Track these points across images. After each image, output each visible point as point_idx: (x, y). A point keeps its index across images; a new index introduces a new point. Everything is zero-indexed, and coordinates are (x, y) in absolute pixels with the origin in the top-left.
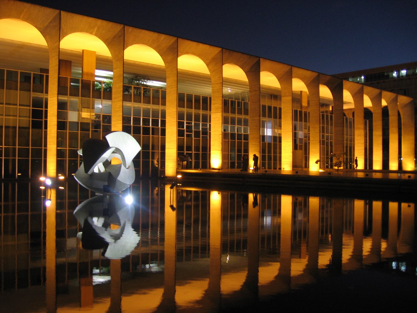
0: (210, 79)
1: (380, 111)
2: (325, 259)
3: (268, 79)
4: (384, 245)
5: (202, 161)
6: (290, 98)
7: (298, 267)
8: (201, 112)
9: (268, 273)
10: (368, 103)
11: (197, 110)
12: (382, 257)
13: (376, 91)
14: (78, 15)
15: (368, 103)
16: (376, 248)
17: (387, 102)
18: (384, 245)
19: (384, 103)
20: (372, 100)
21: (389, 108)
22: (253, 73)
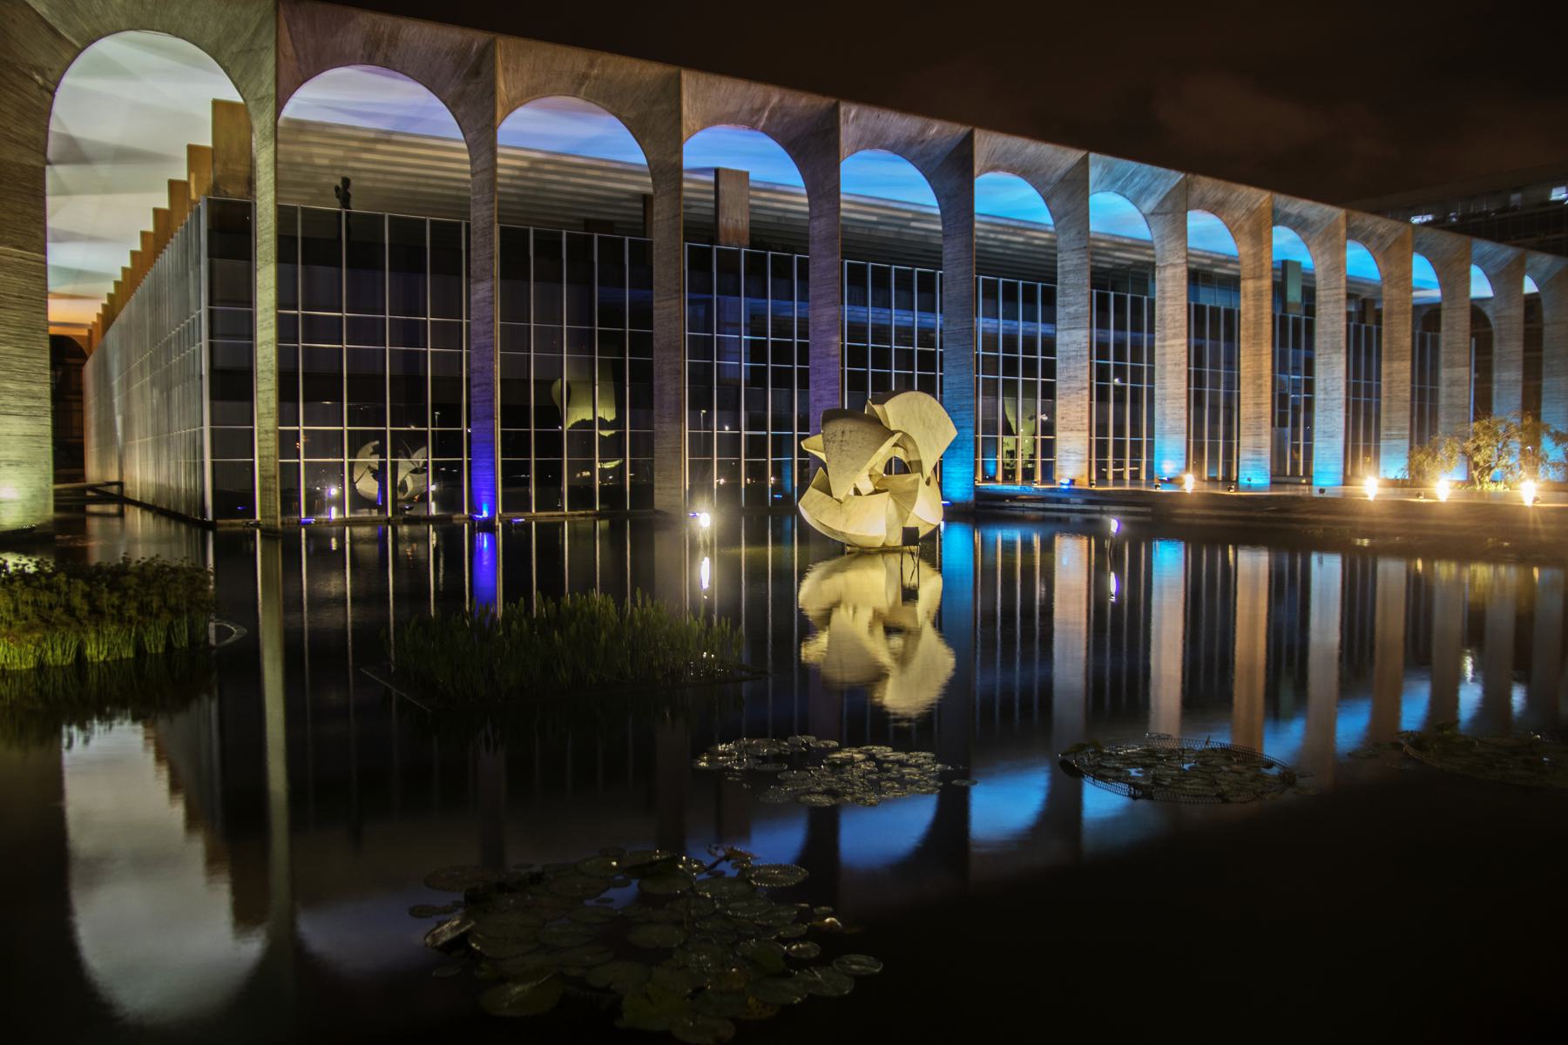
0: (1152, 248)
1: (1517, 312)
2: (1414, 710)
3: (1008, 197)
4: (1518, 697)
5: (214, 464)
6: (1181, 272)
7: (1351, 727)
8: (1040, 329)
9: (1006, 805)
10: (1480, 287)
11: (857, 309)
12: (1088, 840)
13: (1507, 253)
14: (532, 43)
15: (1480, 287)
16: (1494, 701)
17: (1537, 283)
18: (1518, 697)
19: (1529, 287)
20: (1492, 280)
21: (1544, 302)
22: (953, 174)
